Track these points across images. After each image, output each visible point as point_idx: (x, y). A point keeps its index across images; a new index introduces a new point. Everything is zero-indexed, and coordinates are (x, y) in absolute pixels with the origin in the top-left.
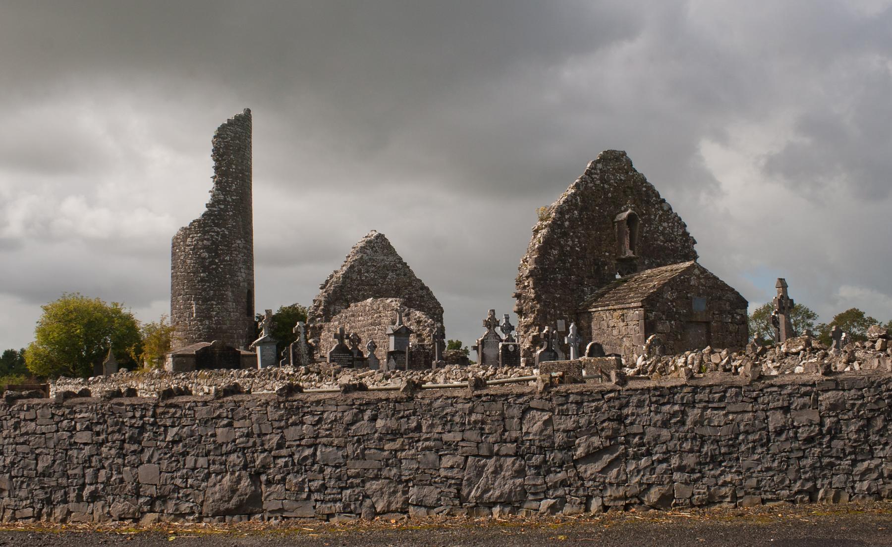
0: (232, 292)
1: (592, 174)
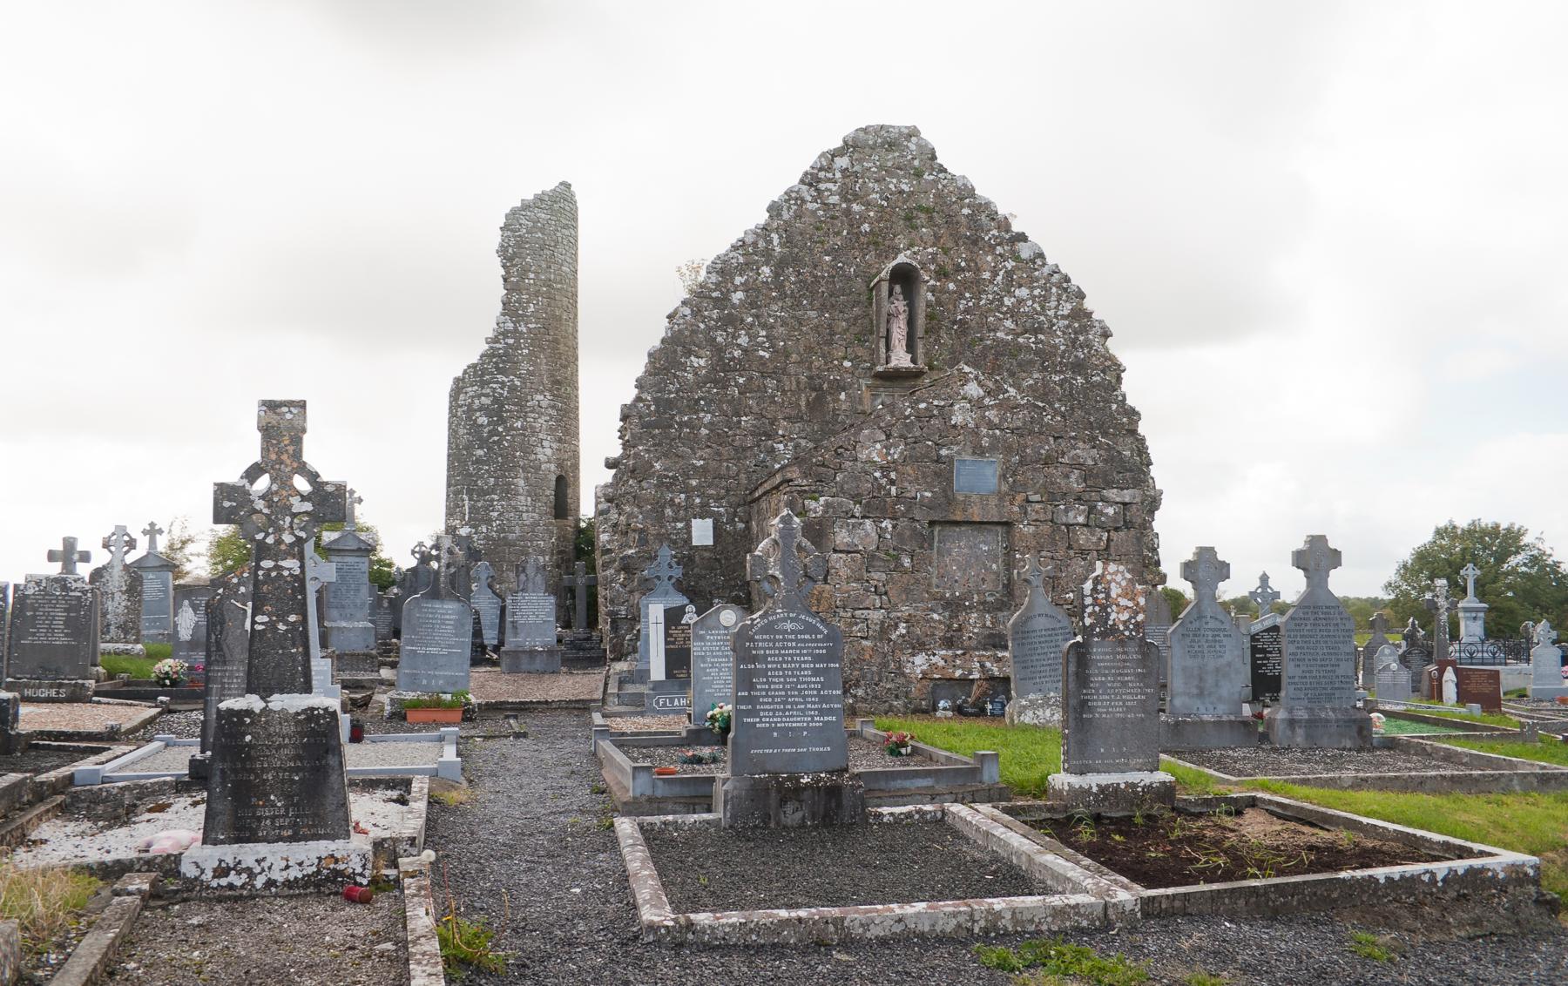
0: (526, 479)
1: (819, 181)
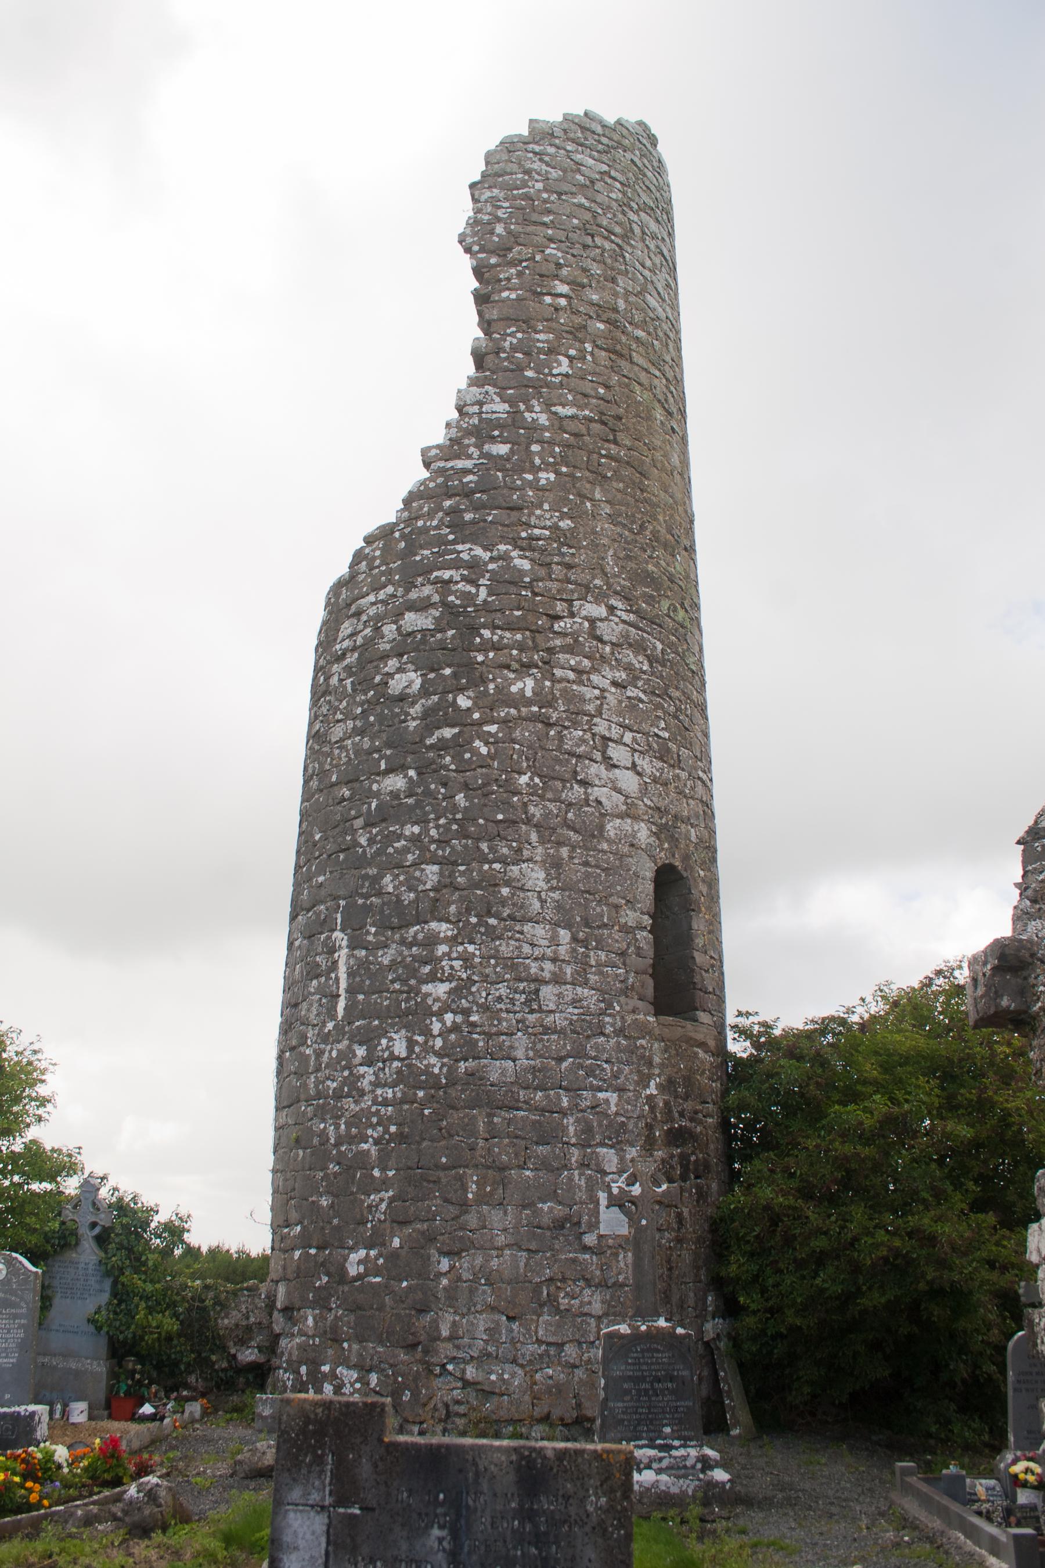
0: (554, 865)
